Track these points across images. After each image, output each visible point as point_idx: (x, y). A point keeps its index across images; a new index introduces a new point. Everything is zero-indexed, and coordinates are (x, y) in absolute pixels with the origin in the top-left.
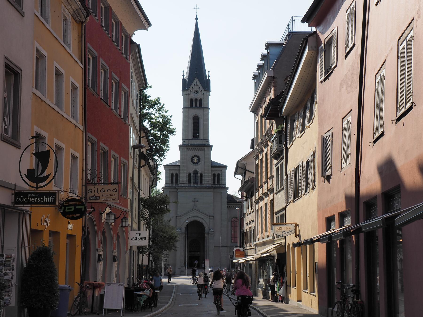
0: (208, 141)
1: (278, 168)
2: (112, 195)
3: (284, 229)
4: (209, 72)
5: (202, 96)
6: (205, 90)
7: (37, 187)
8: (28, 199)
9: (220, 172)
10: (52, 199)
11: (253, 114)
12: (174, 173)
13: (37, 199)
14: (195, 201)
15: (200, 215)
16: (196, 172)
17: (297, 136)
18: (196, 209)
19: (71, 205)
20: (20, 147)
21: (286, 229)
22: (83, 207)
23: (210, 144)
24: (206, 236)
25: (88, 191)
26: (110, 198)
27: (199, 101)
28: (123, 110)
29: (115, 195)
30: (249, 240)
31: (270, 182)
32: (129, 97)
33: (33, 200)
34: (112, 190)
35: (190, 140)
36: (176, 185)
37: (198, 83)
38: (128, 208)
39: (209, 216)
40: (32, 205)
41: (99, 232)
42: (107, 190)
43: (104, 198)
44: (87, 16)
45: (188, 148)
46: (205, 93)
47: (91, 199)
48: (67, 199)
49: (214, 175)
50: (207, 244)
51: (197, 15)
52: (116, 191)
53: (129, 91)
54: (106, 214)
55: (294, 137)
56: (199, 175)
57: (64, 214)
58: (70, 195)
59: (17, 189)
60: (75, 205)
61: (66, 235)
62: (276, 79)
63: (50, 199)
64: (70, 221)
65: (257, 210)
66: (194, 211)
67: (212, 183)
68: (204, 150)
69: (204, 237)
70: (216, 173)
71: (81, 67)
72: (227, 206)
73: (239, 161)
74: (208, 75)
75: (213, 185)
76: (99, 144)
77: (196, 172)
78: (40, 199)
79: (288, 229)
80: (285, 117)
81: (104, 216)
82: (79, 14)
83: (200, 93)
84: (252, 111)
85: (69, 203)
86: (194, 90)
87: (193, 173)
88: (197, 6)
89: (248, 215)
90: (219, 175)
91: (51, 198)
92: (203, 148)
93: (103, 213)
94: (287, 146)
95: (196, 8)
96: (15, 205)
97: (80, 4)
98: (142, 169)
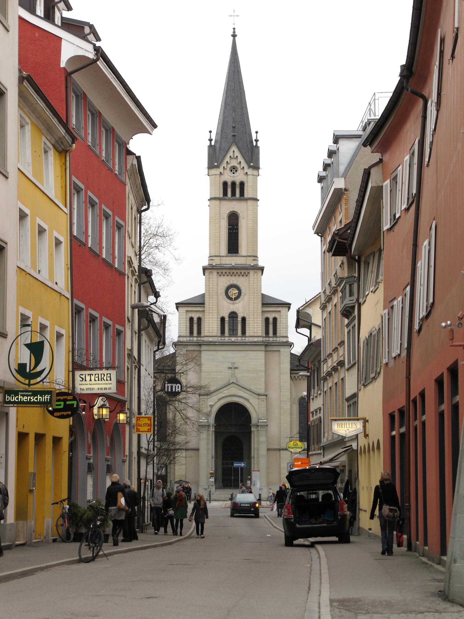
0: (255, 258)
1: (350, 330)
4: (257, 132)
5: (245, 177)
6: (250, 167)
7: (29, 385)
8: (20, 398)
9: (276, 315)
10: (47, 399)
11: (319, 238)
12: (195, 316)
13: (30, 398)
14: (233, 368)
15: (241, 393)
16: (233, 315)
17: (371, 290)
18: (235, 382)
20: (7, 335)
22: (75, 403)
23: (259, 264)
24: (252, 429)
27: (239, 186)
33: (25, 400)
35: (223, 256)
36: (199, 339)
37: (237, 153)
38: (125, 396)
39: (259, 395)
40: (19, 405)
41: (89, 433)
44: (72, 143)
45: (220, 271)
46: (250, 171)
49: (267, 320)
50: (254, 445)
51: (234, 29)
53: (126, 225)
55: (367, 291)
56: (239, 321)
59: (5, 386)
60: (65, 401)
62: (348, 192)
63: (45, 398)
65: (325, 392)
66: (232, 385)
67: (264, 335)
68: (248, 276)
69: (250, 433)
70: (271, 316)
71: (66, 213)
72: (291, 377)
73: (300, 309)
74: (255, 138)
75: (264, 339)
76: (87, 310)
77: (233, 315)
78: (33, 398)
80: (357, 258)
82: (62, 142)
83: (239, 171)
84: (317, 233)
86: (229, 166)
87: (229, 317)
89: (313, 399)
90: (275, 319)
91: (46, 397)
92: (246, 272)
94: (360, 302)
97: (65, 131)
98: (143, 333)
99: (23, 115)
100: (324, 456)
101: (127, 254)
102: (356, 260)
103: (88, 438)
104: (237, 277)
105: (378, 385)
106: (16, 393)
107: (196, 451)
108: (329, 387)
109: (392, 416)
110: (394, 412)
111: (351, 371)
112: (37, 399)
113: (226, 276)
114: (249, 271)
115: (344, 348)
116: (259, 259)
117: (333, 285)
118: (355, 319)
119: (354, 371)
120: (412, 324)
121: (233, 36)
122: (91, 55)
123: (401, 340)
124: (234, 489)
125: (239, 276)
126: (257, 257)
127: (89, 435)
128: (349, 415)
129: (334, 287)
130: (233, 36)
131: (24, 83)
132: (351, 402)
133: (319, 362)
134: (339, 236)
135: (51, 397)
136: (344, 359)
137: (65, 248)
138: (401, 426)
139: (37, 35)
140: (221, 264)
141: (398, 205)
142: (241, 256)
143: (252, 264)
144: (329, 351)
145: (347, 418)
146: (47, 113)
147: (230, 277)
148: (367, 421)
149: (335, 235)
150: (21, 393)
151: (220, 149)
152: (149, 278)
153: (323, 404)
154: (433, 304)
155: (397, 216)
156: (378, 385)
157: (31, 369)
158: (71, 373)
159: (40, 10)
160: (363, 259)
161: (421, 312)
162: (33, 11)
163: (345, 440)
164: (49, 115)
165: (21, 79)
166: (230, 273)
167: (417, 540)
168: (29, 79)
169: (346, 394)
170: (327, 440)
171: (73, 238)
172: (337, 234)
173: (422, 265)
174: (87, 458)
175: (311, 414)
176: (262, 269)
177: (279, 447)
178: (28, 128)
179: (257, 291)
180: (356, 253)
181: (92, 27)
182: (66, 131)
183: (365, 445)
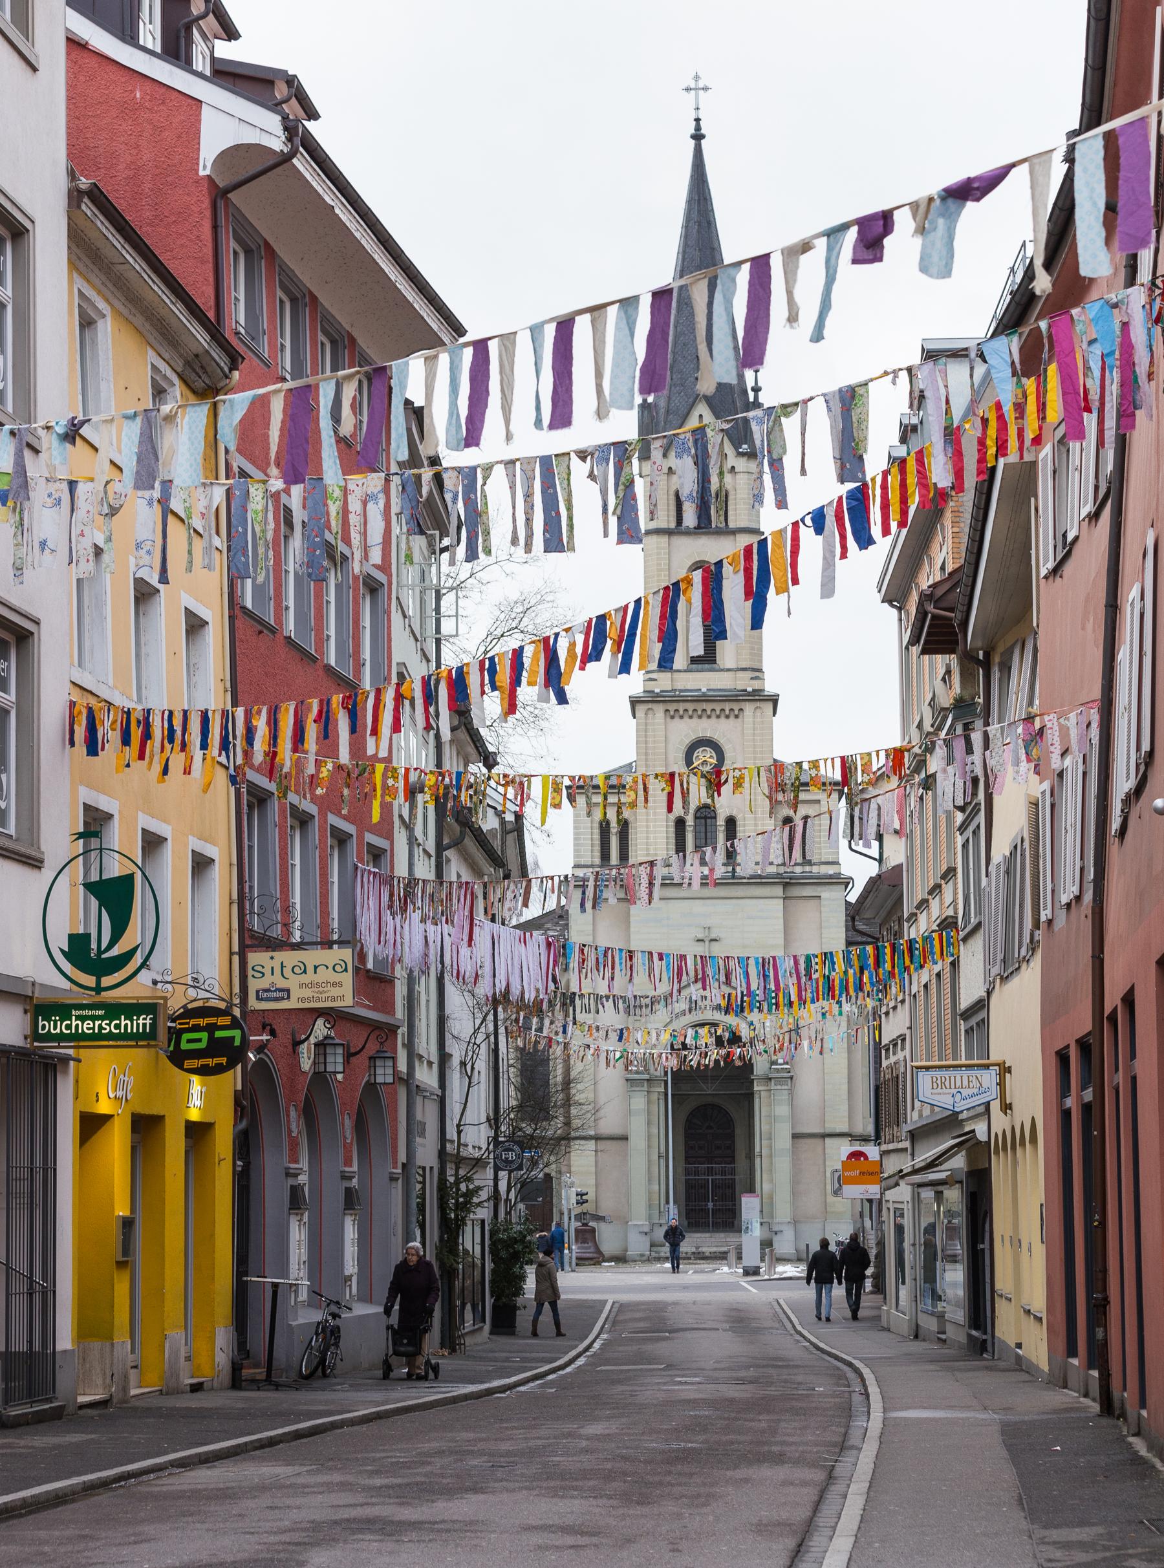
0: (757, 674)
1: (967, 840)
2: (334, 985)
3: (958, 1084)
7: (98, 989)
8: (74, 1024)
10: (144, 1025)
11: (895, 612)
13: (100, 1025)
19: (196, 1028)
20: (42, 862)
21: (965, 1083)
22: (237, 1033)
24: (756, 1088)
25: (250, 972)
26: (327, 995)
28: (366, 654)
29: (340, 984)
30: (893, 1118)
31: (948, 890)
32: (389, 605)
34: (331, 968)
40: (82, 1044)
41: (292, 1109)
42: (316, 967)
43: (307, 993)
44: (231, 370)
45: (672, 707)
47: (262, 999)
48: (184, 1007)
50: (761, 1125)
51: (698, 120)
52: (346, 970)
53: (390, 583)
54: (316, 1045)
57: (178, 1058)
58: (192, 993)
60: (211, 1029)
61: (183, 1124)
63: (138, 1025)
64: (196, 1079)
65: (915, 996)
78: (109, 1025)
79: (974, 1082)
81: (309, 1049)
82: (202, 367)
84: (888, 600)
85: (193, 1022)
88: (697, 78)
91: (141, 1022)
92: (736, 707)
93: (303, 1042)
95: (693, 86)
96: (36, 1044)
97: (208, 338)
99: (90, 293)
100: (913, 1155)
101: (396, 658)
102: (978, 662)
103: (289, 1121)
104: (714, 720)
105: (1030, 979)
106: (63, 1010)
107: (620, 1142)
108: (923, 983)
109: (1063, 1058)
110: (1068, 1046)
111: (971, 942)
112: (117, 1027)
113: (686, 719)
114: (742, 705)
115: (955, 884)
116: (766, 676)
117: (927, 727)
118: (979, 810)
119: (977, 943)
120: (1106, 815)
121: (693, 137)
122: (277, 143)
123: (1082, 858)
124: (713, 1231)
125: (718, 717)
126: (760, 670)
127: (293, 1113)
128: (969, 1056)
129: (929, 733)
130: (693, 137)
131: (83, 207)
132: (973, 1022)
133: (900, 920)
134: (935, 602)
135: (154, 1020)
136: (956, 913)
137: (215, 639)
138: (1084, 1088)
139: (138, 95)
140: (674, 690)
141: (1073, 508)
142: (722, 670)
143: (750, 689)
144: (919, 895)
145: (963, 1061)
146: (156, 288)
147: (695, 720)
148: (1009, 1070)
149: (924, 598)
150: (78, 1013)
151: (668, 412)
152: (463, 719)
153: (908, 1025)
154: (1151, 754)
155: (1070, 537)
156: (1030, 979)
157: (103, 948)
158: (236, 958)
159: (150, 32)
160: (996, 659)
161: (1123, 783)
162: (129, 36)
163: (961, 1117)
164: (160, 293)
165: (75, 197)
166: (695, 710)
167: (1125, 1389)
168: (96, 196)
169: (962, 1000)
170: (920, 1115)
171: (237, 611)
172: (932, 595)
173: (1125, 655)
174: (288, 1175)
175: (883, 1052)
176: (774, 700)
177: (822, 1131)
178: (107, 329)
179: (762, 752)
180: (979, 644)
181: (291, 81)
182: (213, 337)
183: (1033, 1119)
